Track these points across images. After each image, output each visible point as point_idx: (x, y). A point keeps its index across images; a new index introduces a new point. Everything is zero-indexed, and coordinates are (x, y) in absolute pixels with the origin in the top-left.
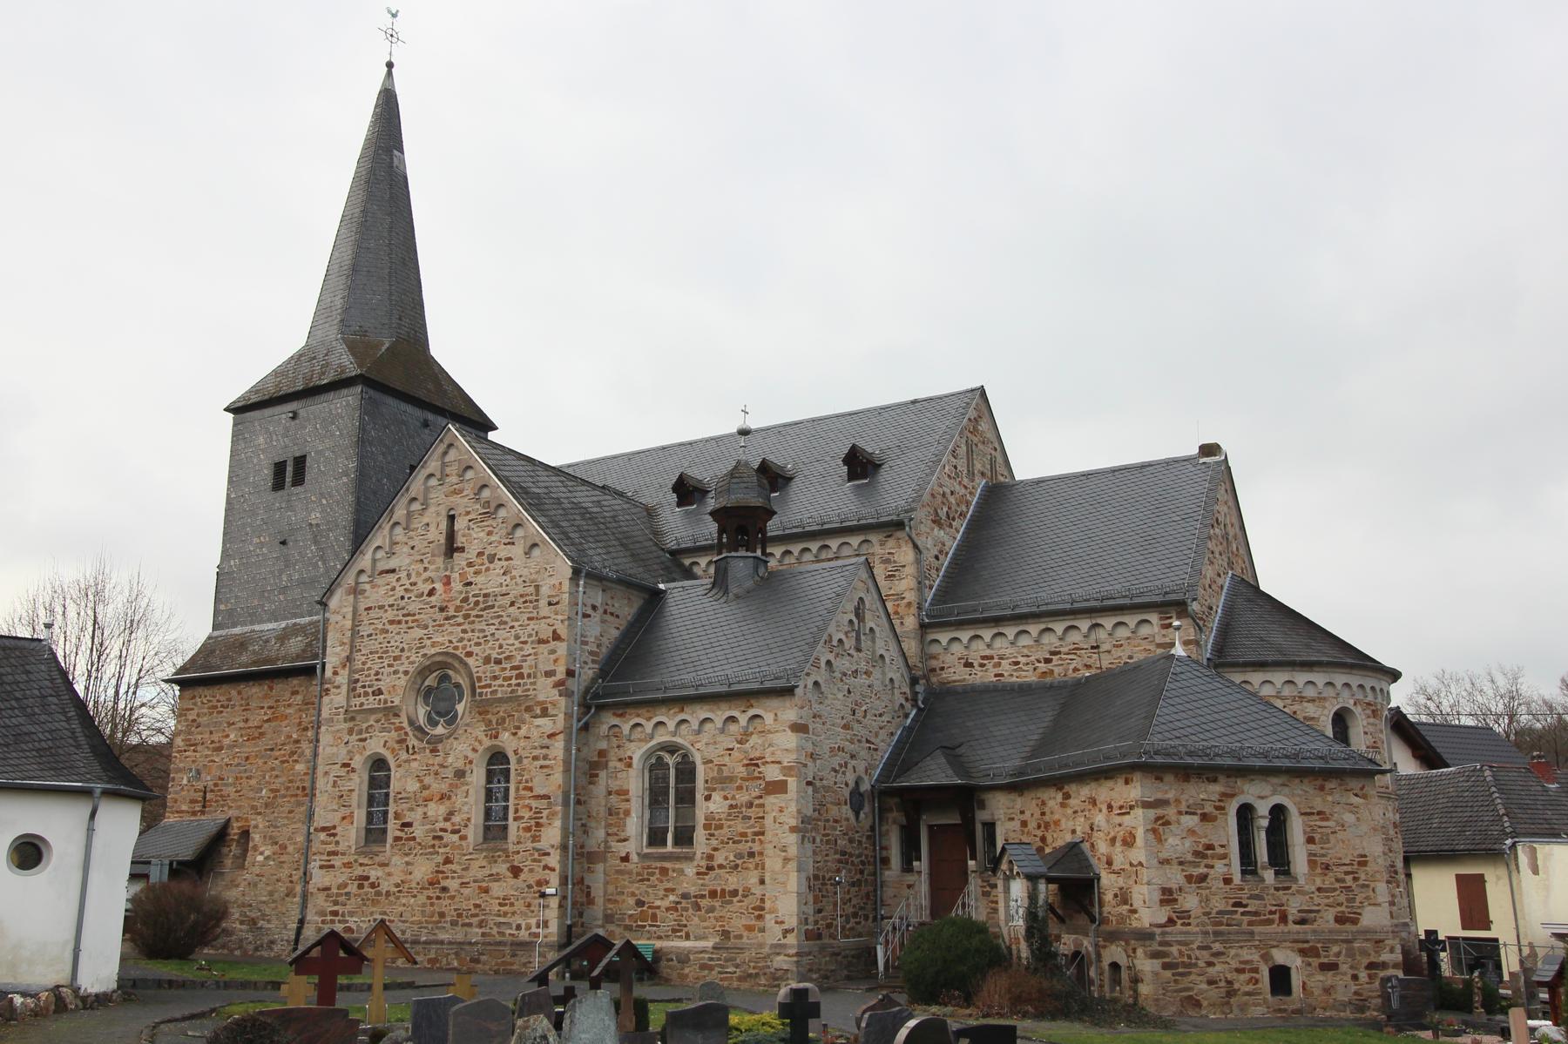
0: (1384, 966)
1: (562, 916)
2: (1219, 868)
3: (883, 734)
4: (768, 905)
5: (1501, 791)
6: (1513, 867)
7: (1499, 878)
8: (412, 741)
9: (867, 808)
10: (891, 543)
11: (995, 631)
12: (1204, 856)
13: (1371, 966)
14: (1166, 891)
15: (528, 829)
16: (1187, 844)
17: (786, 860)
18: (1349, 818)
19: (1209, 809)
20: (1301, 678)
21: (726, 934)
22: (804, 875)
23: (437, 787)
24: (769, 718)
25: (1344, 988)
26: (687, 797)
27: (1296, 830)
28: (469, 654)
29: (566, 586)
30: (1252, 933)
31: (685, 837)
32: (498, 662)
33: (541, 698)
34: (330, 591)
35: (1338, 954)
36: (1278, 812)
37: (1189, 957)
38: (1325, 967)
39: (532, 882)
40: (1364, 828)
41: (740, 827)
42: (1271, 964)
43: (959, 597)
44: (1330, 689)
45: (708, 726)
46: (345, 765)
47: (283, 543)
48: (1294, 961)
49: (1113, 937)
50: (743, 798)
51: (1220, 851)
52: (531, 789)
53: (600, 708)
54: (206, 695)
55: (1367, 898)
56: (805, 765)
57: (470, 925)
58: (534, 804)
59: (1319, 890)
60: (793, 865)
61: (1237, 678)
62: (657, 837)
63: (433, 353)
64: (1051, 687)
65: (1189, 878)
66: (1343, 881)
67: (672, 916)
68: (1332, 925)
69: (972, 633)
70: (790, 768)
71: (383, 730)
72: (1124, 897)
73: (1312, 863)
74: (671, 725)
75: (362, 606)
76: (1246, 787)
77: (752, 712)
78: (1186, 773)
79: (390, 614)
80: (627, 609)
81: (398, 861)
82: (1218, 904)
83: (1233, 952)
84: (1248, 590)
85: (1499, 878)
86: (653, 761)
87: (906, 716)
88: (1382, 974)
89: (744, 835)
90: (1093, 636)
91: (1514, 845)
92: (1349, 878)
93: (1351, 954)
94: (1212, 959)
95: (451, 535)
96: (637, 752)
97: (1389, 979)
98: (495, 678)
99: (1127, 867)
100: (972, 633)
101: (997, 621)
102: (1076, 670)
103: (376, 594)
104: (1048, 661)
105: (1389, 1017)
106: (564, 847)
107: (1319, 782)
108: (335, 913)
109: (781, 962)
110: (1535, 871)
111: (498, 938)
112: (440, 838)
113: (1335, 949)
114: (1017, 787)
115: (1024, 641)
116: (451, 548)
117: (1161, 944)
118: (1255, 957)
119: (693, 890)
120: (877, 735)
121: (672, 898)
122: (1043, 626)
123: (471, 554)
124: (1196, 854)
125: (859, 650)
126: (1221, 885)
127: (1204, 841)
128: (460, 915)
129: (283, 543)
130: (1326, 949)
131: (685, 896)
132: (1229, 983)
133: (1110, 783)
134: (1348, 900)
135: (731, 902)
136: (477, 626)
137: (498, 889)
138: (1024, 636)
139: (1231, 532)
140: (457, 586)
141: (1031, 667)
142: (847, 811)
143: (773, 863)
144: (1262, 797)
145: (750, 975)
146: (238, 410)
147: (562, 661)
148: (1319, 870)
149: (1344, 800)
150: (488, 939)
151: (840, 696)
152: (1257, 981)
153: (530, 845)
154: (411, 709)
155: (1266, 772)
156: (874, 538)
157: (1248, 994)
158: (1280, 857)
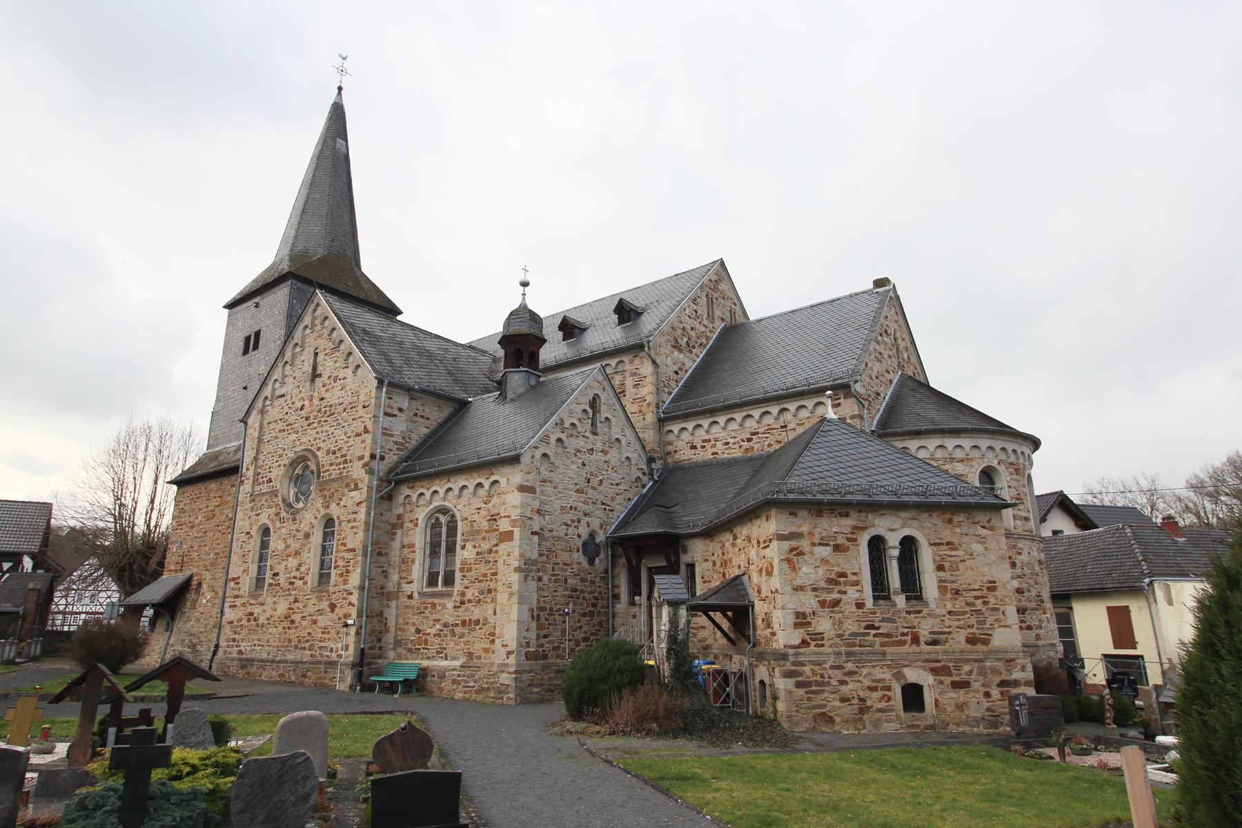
0: (1016, 683)
1: (357, 642)
2: (852, 594)
3: (619, 499)
4: (497, 631)
5: (1139, 543)
6: (1151, 599)
7: (1140, 609)
8: (283, 514)
9: (602, 556)
10: (637, 361)
11: (711, 420)
12: (837, 583)
13: (1002, 684)
14: (798, 615)
15: (341, 575)
16: (821, 571)
18: (977, 548)
19: (841, 540)
20: (950, 443)
21: (470, 655)
22: (526, 608)
23: (295, 546)
24: (503, 482)
25: (977, 706)
26: (451, 550)
27: (926, 559)
28: (319, 449)
29: (374, 391)
30: (884, 654)
31: (449, 580)
32: (334, 453)
33: (355, 476)
34: (248, 413)
35: (970, 672)
36: (909, 545)
37: (822, 676)
38: (956, 685)
39: (341, 615)
40: (992, 556)
41: (483, 569)
42: (903, 682)
43: (692, 399)
44: (976, 451)
45: (466, 492)
46: (248, 533)
47: (245, 388)
49: (761, 657)
50: (486, 546)
51: (851, 578)
52: (344, 545)
53: (399, 483)
54: (191, 490)
55: (998, 620)
56: (531, 519)
57: (304, 648)
58: (347, 555)
59: (950, 613)
60: (515, 599)
61: (899, 445)
62: (432, 581)
64: (751, 459)
65: (822, 603)
66: (974, 605)
67: (437, 640)
69: (695, 423)
70: (516, 521)
71: (269, 507)
72: (768, 623)
73: (942, 589)
74: (442, 492)
75: (266, 422)
76: (877, 521)
77: (493, 478)
78: (818, 508)
79: (280, 426)
80: (437, 414)
81: (269, 600)
82: (851, 627)
83: (865, 671)
84: (916, 385)
85: (1140, 609)
87: (644, 486)
88: (1014, 691)
89: (485, 575)
90: (782, 419)
91: (1151, 582)
92: (979, 602)
93: (982, 672)
94: (845, 678)
95: (315, 368)
96: (421, 514)
97: (1017, 697)
98: (332, 464)
99: (769, 594)
100: (695, 423)
101: (712, 412)
102: (770, 445)
103: (274, 413)
104: (749, 440)
105: (1018, 734)
106: (362, 588)
107: (948, 516)
108: (234, 640)
109: (506, 679)
110: (1170, 603)
111: (319, 659)
112: (292, 583)
113: (967, 668)
114: (709, 533)
115: (733, 426)
116: (315, 375)
117: (794, 664)
118: (888, 676)
119: (451, 620)
120: (613, 499)
121: (438, 627)
122: (745, 414)
124: (830, 581)
125: (595, 433)
126: (854, 609)
127: (837, 569)
128: (299, 641)
129: (245, 388)
130: (958, 668)
131: (446, 625)
132: (862, 700)
133: (758, 522)
134: (978, 622)
135: (474, 630)
136: (324, 428)
137: (322, 621)
138: (732, 423)
139: (902, 345)
140: (316, 401)
141: (737, 446)
142: (579, 557)
143: (502, 597)
144: (893, 530)
145: (483, 689)
146: (230, 306)
147: (368, 449)
148: (949, 595)
149: (972, 532)
150: (314, 660)
151: (574, 467)
152: (889, 699)
153: (342, 587)
154: (285, 491)
155: (896, 507)
156: (626, 359)
157: (880, 710)
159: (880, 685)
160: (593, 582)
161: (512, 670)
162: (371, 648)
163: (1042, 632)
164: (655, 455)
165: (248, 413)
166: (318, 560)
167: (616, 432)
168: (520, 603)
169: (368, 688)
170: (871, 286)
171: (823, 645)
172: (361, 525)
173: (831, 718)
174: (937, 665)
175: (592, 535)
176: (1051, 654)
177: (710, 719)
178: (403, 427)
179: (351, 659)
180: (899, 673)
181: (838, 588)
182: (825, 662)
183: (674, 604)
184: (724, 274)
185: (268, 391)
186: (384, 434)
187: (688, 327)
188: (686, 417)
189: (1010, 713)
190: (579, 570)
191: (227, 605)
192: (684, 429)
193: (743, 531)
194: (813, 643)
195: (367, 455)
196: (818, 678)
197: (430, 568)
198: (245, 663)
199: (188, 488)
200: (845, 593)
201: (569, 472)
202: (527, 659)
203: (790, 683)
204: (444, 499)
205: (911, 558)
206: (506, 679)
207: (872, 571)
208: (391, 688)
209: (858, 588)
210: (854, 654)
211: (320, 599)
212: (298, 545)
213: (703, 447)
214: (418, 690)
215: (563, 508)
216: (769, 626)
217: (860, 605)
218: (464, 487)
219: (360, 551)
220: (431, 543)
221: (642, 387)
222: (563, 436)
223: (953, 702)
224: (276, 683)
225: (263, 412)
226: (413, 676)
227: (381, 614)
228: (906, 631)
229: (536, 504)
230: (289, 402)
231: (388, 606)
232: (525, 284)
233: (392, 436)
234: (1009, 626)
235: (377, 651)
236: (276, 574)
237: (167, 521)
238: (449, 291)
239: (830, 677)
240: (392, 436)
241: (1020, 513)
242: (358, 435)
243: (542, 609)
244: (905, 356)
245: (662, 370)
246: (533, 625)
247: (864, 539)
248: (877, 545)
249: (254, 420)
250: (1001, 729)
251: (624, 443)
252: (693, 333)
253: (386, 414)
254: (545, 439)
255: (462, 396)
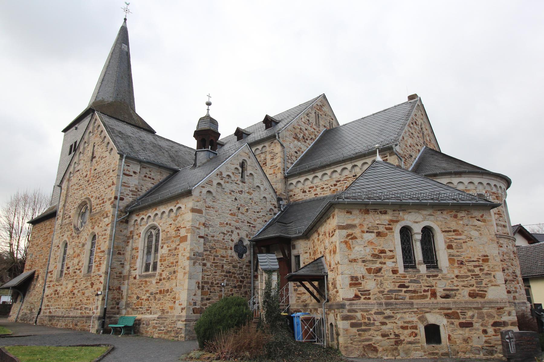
0: (505, 324)
1: (103, 304)
2: (390, 264)
4: (177, 296)
8: (74, 234)
9: (248, 253)
10: (273, 145)
11: (314, 175)
12: (379, 257)
13: (495, 324)
14: (352, 278)
15: (97, 266)
17: (185, 273)
19: (382, 229)
21: (163, 311)
22: (194, 282)
23: (78, 251)
25: (478, 340)
26: (156, 250)
27: (440, 241)
29: (118, 161)
30: (412, 304)
33: (107, 210)
34: (62, 182)
35: (473, 317)
36: (427, 232)
37: (369, 319)
38: (463, 325)
40: (485, 239)
41: (172, 259)
42: (425, 323)
43: (305, 166)
44: (471, 185)
45: (165, 215)
46: (58, 246)
48: (441, 321)
49: (330, 308)
50: (174, 246)
52: (100, 249)
53: (131, 213)
54: (38, 226)
56: (199, 229)
57: (78, 309)
58: (101, 255)
59: (457, 276)
60: (187, 276)
62: (147, 269)
63: (196, 141)
65: (369, 270)
66: (473, 271)
68: (467, 298)
70: (189, 229)
71: (68, 231)
72: (334, 285)
73: (451, 260)
74: (152, 216)
75: (70, 185)
77: (178, 206)
79: (76, 187)
80: (158, 177)
82: (389, 286)
83: (399, 316)
86: (149, 234)
87: (275, 214)
88: (503, 329)
89: (172, 263)
90: (353, 171)
92: (477, 270)
94: (385, 321)
95: (93, 154)
96: (142, 230)
98: (97, 205)
100: (305, 178)
101: (314, 170)
103: (74, 180)
106: (106, 273)
107: (454, 213)
108: (48, 306)
111: (84, 315)
113: (470, 313)
115: (326, 178)
116: (93, 157)
117: (349, 311)
119: (154, 290)
120: (255, 220)
121: (148, 295)
122: (332, 170)
123: (97, 157)
126: (391, 274)
127: (380, 248)
130: (464, 314)
131: (151, 294)
132: (397, 335)
133: (328, 221)
134: (477, 283)
135: (166, 296)
136: (95, 185)
137: (88, 293)
139: (426, 133)
140: (92, 171)
143: (180, 275)
144: (417, 222)
146: (65, 131)
147: (114, 194)
148: (456, 265)
149: (470, 223)
151: (229, 200)
152: (416, 335)
153: (97, 273)
156: (267, 144)
157: (410, 343)
158: (430, 259)
159: (409, 325)
160: (241, 268)
161: (184, 319)
162: (112, 308)
163: (517, 295)
164: (282, 197)
165: (62, 182)
166: (88, 259)
167: (257, 182)
168: (190, 278)
169: (107, 331)
170: (406, 100)
171: (369, 299)
172: (108, 237)
173: (375, 348)
174: (449, 311)
175: (241, 241)
176: (524, 308)
177: (288, 349)
178: (136, 182)
179: (99, 314)
180: (423, 317)
181: (380, 260)
182: (371, 310)
183: (269, 272)
184: (325, 103)
185: (71, 169)
186: (122, 185)
187: (304, 129)
188: (300, 174)
189: (503, 345)
190: (232, 261)
191: (46, 286)
192: (299, 182)
193: (322, 230)
194: (363, 297)
195: (113, 197)
196: (366, 321)
197: (146, 261)
198: (51, 318)
199: (37, 225)
200: (385, 263)
201: (225, 203)
202: (194, 313)
203: (347, 323)
204: (154, 220)
205: (430, 241)
206: (180, 325)
207: (403, 250)
208: (117, 331)
209: (394, 260)
210: (391, 304)
211: (87, 280)
212: (79, 251)
213: (309, 191)
214: (135, 333)
215: (221, 224)
216: (335, 287)
217: (395, 272)
218: (164, 212)
219: (106, 252)
220: (148, 247)
221: (275, 159)
222: (222, 182)
223: (461, 337)
224: (64, 329)
225: (69, 180)
226: (131, 324)
227: (119, 288)
228: (427, 288)
229: (203, 220)
230: (81, 173)
231: (123, 284)
232: (209, 104)
233: (129, 187)
234: (498, 285)
235: (116, 310)
236: (68, 268)
237: (23, 243)
238: (169, 113)
239: (374, 320)
240: (129, 187)
241: (500, 222)
242: (109, 186)
243: (207, 283)
244: (428, 139)
245: (287, 150)
246: (199, 292)
247: (397, 228)
248: (406, 232)
249: (64, 185)
250: (496, 355)
251: (262, 188)
252: (306, 132)
253: (124, 174)
254: (210, 183)
255: (176, 167)
